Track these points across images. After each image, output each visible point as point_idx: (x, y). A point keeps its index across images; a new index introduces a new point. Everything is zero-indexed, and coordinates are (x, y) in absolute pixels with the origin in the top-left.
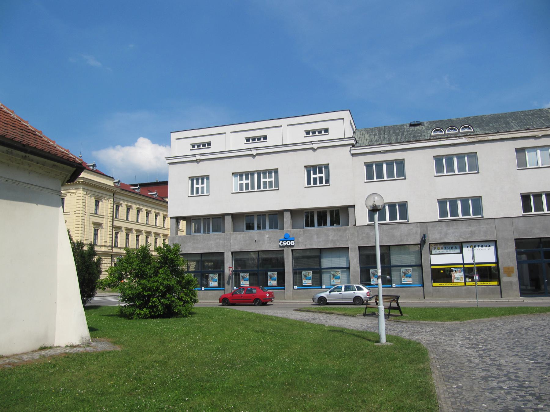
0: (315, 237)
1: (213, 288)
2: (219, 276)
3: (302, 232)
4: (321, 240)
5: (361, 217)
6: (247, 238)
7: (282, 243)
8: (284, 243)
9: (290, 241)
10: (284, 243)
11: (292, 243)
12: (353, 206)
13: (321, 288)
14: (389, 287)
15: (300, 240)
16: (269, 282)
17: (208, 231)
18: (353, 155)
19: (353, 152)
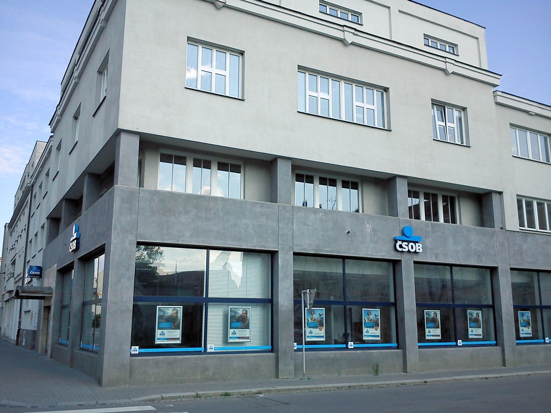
0: (451, 240)
1: (372, 345)
2: (385, 317)
3: (430, 229)
4: (460, 248)
5: (510, 216)
6: (331, 225)
7: (401, 246)
8: (404, 244)
9: (415, 242)
10: (404, 244)
11: (418, 247)
12: (500, 193)
13: (347, 348)
14: (199, 353)
15: (428, 242)
16: (158, 332)
17: (436, 218)
18: (498, 104)
19: (500, 100)
